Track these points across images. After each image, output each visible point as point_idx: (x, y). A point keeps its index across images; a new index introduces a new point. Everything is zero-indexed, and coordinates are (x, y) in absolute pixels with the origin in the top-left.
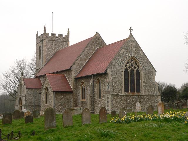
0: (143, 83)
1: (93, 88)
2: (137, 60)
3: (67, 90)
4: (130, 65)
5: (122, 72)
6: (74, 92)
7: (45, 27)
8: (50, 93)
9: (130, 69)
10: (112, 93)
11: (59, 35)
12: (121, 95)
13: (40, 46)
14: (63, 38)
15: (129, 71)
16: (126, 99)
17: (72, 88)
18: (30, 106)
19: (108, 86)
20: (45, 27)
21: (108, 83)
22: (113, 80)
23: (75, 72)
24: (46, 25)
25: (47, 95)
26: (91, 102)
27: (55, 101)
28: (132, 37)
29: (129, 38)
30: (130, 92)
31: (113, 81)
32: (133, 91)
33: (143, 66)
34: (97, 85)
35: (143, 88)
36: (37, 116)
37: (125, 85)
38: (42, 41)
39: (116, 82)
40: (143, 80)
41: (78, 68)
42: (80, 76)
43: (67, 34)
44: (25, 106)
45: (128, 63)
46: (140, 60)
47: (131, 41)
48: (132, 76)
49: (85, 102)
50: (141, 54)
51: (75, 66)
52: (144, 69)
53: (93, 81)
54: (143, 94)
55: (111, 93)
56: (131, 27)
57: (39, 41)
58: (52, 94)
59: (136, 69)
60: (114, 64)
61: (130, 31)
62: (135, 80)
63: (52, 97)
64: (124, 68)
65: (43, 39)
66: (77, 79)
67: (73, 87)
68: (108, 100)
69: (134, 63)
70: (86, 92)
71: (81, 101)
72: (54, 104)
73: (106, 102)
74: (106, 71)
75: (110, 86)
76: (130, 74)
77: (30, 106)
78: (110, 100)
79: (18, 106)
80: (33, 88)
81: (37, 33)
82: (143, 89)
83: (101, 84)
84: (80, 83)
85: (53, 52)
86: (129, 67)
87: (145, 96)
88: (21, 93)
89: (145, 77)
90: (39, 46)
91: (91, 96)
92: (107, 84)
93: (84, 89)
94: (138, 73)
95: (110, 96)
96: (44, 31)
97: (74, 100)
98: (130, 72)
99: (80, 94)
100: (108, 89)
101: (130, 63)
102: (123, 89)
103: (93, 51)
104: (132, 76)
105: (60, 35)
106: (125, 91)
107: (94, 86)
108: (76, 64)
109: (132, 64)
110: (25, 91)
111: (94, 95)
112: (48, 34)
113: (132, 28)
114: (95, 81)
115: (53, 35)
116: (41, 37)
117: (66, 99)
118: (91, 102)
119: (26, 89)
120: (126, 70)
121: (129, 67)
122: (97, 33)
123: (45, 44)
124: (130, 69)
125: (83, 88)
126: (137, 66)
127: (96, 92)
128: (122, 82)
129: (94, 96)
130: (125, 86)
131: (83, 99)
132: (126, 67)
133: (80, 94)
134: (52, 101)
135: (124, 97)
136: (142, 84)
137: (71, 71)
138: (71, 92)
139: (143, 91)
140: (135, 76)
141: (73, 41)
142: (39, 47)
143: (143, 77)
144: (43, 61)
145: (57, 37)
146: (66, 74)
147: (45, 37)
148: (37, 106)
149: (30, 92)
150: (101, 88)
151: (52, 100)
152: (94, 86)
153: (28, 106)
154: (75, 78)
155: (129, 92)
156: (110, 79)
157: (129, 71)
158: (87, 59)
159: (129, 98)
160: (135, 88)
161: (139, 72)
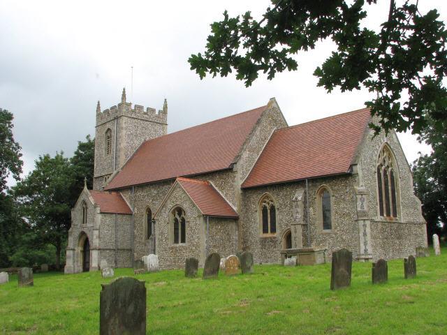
11: (148, 109)
15: (382, 172)
18: (107, 249)
19: (363, 201)
23: (241, 176)
24: (126, 88)
30: (392, 216)
32: (388, 215)
36: (249, 268)
43: (162, 109)
44: (99, 249)
51: (241, 162)
56: (62, 153)
57: (100, 123)
66: (246, 190)
68: (365, 231)
70: (278, 217)
71: (261, 238)
73: (361, 234)
77: (107, 249)
80: (112, 211)
81: (99, 105)
85: (138, 143)
92: (360, 196)
100: (362, 207)
105: (151, 110)
119: (101, 213)
133: (258, 221)
138: (235, 219)
141: (174, 125)
146: (212, 179)
148: (121, 250)
149: (108, 219)
157: (382, 172)
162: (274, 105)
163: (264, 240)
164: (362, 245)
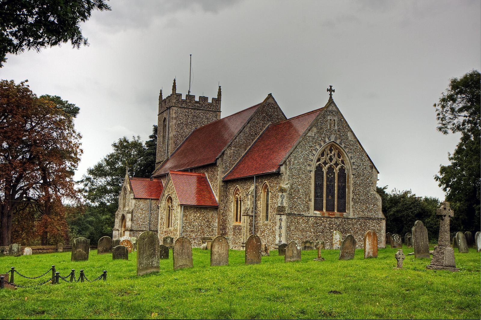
0: (351, 195)
1: (256, 201)
2: (342, 150)
3: (209, 203)
4: (328, 158)
5: (311, 171)
6: (222, 207)
7: (174, 83)
8: (175, 208)
9: (327, 166)
10: (289, 212)
12: (306, 215)
13: (165, 119)
14: (209, 104)
15: (325, 170)
16: (317, 223)
17: (217, 199)
20: (174, 83)
21: (282, 190)
22: (291, 186)
25: (170, 210)
26: (249, 227)
27: (183, 223)
28: (333, 105)
29: (327, 106)
30: (324, 210)
31: (292, 188)
32: (330, 208)
33: (352, 161)
34: (262, 195)
35: (352, 203)
37: (316, 196)
38: (169, 108)
39: (299, 190)
40: (352, 189)
41: (230, 162)
42: (232, 177)
45: (322, 155)
46: (346, 150)
47: (331, 112)
48: (330, 181)
49: (240, 226)
50: (350, 139)
52: (354, 167)
53: (256, 187)
54: (351, 216)
55: (287, 211)
56: (331, 87)
58: (179, 210)
59: (339, 166)
60: (295, 157)
61: (329, 93)
62: (336, 189)
63: (179, 215)
64: (314, 164)
65: (171, 104)
67: (220, 198)
68: (281, 224)
69: (334, 155)
72: (181, 228)
74: (279, 168)
75: (285, 198)
76: (327, 176)
78: (283, 224)
79: (118, 230)
81: (161, 94)
82: (351, 206)
83: (270, 194)
84: (232, 190)
86: (325, 163)
87: (355, 219)
88: (124, 206)
89: (355, 184)
90: (164, 118)
91: (250, 216)
93: (239, 202)
94: (342, 174)
95: (284, 217)
96: (173, 89)
97: (221, 223)
98: (327, 173)
99: (232, 211)
100: (282, 203)
101: (328, 155)
102: (312, 204)
103: (261, 129)
104: (330, 181)
105: (204, 99)
106: (315, 209)
107: (256, 197)
108: (227, 154)
109: (331, 156)
110: (132, 203)
111: (256, 213)
112: (180, 95)
113: (333, 88)
114: (260, 188)
115: (190, 97)
116: (167, 100)
117: (206, 220)
118: (249, 227)
119: (135, 198)
120: (319, 169)
121: (325, 163)
122: (270, 95)
123: (174, 116)
124: (327, 166)
125: (237, 199)
126: (340, 162)
127: (261, 209)
128: (311, 191)
129: (255, 216)
130: (315, 200)
131: (237, 221)
132: (318, 163)
133: (232, 211)
134: (179, 223)
135: (312, 220)
136: (350, 195)
137: (217, 166)
139: (351, 209)
140: (336, 181)
142: (163, 120)
143: (352, 182)
144: (170, 148)
145: (197, 102)
146: (207, 171)
147: (175, 101)
149: (142, 204)
150: (270, 202)
151: (179, 222)
152: (256, 197)
153: (136, 231)
154: (224, 181)
155: (322, 210)
156: (287, 184)
157: (325, 170)
158: (247, 146)
159: (323, 222)
160: (336, 203)
161: (345, 174)
162: (270, 100)
163: (235, 227)
164: (277, 237)
